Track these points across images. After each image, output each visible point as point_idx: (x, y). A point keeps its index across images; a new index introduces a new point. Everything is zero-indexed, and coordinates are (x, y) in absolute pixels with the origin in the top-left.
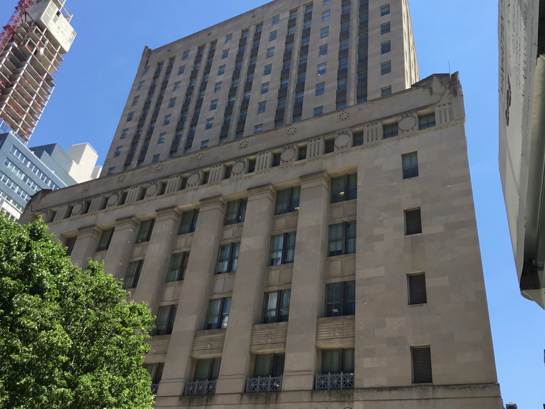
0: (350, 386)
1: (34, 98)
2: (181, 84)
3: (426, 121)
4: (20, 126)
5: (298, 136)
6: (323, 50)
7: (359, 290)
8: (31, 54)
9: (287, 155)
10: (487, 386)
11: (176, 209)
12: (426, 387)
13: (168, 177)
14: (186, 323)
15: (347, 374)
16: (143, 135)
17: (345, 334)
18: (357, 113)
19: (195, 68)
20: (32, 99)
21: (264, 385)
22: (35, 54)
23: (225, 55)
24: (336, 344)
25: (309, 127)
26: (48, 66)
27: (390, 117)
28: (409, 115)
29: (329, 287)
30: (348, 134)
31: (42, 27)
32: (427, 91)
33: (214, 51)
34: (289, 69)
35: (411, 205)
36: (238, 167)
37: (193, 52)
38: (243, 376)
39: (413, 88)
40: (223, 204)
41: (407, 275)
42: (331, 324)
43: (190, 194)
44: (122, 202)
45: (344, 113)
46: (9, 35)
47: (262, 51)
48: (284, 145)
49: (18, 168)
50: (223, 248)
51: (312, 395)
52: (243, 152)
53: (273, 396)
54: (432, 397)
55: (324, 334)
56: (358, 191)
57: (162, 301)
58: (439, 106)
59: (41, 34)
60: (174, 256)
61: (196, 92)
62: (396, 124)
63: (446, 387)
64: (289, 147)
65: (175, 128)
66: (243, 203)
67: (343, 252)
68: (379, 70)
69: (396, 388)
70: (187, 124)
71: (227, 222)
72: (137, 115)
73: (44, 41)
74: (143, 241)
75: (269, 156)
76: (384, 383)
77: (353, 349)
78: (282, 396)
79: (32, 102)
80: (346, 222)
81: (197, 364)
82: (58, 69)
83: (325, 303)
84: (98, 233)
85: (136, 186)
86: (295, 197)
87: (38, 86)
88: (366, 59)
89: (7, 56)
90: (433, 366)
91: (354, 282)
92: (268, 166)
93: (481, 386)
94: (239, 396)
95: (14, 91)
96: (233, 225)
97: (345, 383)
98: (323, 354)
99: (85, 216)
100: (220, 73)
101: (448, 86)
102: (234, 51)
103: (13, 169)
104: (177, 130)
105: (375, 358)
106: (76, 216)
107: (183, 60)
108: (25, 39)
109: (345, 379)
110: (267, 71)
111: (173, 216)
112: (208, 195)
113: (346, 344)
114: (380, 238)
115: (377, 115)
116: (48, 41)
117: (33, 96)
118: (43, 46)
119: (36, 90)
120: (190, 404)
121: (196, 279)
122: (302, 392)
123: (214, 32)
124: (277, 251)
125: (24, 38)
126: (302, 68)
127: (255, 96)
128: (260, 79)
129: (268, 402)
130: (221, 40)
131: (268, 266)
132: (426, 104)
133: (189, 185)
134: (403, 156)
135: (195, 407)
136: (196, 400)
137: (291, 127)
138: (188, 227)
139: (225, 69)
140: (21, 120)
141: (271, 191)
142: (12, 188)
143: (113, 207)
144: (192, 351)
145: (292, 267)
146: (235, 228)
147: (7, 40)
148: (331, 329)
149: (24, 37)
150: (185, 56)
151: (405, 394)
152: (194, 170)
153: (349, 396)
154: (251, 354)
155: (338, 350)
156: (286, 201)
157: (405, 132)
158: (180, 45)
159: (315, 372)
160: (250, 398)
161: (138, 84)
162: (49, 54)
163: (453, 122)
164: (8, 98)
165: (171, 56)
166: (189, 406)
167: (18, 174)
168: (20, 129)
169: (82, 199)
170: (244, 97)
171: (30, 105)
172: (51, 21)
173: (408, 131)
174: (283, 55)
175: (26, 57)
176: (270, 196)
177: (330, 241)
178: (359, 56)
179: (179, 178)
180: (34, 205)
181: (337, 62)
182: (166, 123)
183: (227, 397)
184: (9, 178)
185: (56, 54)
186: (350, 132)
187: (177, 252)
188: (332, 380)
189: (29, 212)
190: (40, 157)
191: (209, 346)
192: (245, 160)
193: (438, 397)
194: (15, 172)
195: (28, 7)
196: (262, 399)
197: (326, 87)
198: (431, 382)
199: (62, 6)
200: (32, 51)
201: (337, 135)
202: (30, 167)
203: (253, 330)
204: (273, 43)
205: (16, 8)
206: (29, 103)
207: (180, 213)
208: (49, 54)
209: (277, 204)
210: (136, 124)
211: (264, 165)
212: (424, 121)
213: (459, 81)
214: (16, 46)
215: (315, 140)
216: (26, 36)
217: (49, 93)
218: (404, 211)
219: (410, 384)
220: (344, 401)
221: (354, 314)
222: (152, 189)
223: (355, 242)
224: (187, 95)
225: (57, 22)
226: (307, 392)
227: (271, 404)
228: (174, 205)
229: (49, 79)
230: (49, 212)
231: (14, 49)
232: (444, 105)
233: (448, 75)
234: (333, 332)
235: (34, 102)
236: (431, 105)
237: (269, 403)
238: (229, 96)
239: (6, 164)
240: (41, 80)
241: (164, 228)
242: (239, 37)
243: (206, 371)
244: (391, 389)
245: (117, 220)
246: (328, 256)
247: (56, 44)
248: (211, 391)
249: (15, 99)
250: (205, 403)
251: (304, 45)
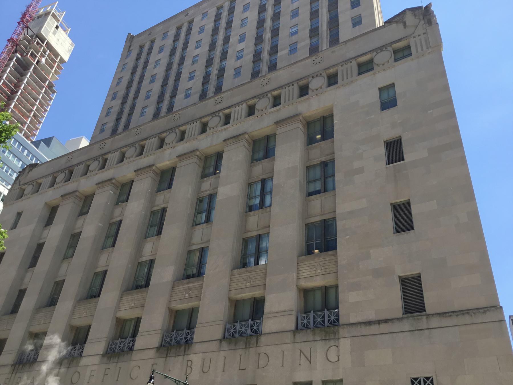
0: (335, 323)
1: (37, 103)
2: (161, 62)
3: (402, 53)
4: (25, 129)
5: (274, 85)
6: (295, 14)
7: (340, 225)
8: (33, 64)
9: (261, 104)
10: (488, 310)
11: (154, 168)
12: (420, 317)
13: (146, 139)
14: (164, 274)
15: (332, 311)
16: (126, 111)
17: (327, 270)
18: (330, 56)
19: (174, 46)
20: (35, 104)
21: (243, 329)
22: (37, 63)
23: (202, 30)
24: (319, 282)
25: (282, 76)
26: (50, 74)
27: (365, 54)
28: (384, 49)
29: (308, 227)
30: (322, 76)
31: (43, 39)
32: (401, 26)
33: (191, 29)
34: (263, 35)
35: (391, 135)
36: (213, 122)
37: (172, 32)
38: (221, 322)
39: (386, 25)
40: (200, 158)
41: (391, 204)
42: (311, 262)
43: (168, 152)
44: (103, 167)
45: (317, 57)
46: (12, 47)
47: (236, 22)
48: (258, 95)
49: (15, 156)
50: (200, 200)
51: (294, 335)
52: (219, 107)
53: (254, 340)
54: (426, 328)
55: (305, 272)
56: (335, 128)
57: (141, 257)
58: (414, 37)
59: (42, 46)
60: (153, 213)
61: (175, 67)
62: (371, 61)
63: (442, 315)
64: (263, 97)
65: (156, 101)
66: (219, 156)
67: (323, 191)
68: (350, 24)
69: (386, 321)
70: (167, 96)
71: (204, 176)
72: (121, 93)
73: (45, 52)
74: (122, 202)
75: (244, 108)
76: (372, 316)
77: (336, 287)
78: (263, 339)
79: (36, 107)
80: (324, 162)
81: (175, 315)
82: (59, 77)
83: (306, 243)
84: (81, 199)
85: (116, 150)
86: (271, 145)
87: (41, 93)
88: (337, 16)
89: (11, 66)
90: (425, 295)
91: (334, 219)
92: (243, 117)
93: (481, 311)
94: (217, 343)
95: (19, 98)
96: (211, 177)
97: (329, 320)
98: (305, 293)
99: (68, 184)
100: (197, 47)
101: (421, 17)
102: (210, 26)
103: (11, 157)
104: (158, 103)
105: (361, 291)
106: (60, 185)
107: (162, 40)
108: (28, 50)
109: (329, 317)
110: (242, 39)
111: (151, 174)
112: (186, 151)
113: (329, 281)
114: (361, 171)
115: (352, 54)
116: (48, 52)
117: (36, 101)
118: (44, 57)
119: (39, 96)
120: (167, 355)
121: (173, 232)
122: (283, 333)
123: (191, 12)
124: (255, 197)
125: (26, 49)
126: (275, 32)
127: (231, 64)
128: (235, 46)
129: (248, 347)
130: (197, 19)
131: (246, 212)
132: (400, 38)
133: (167, 144)
134: (380, 90)
135: (173, 358)
136: (173, 351)
137: (265, 78)
138: (166, 184)
139: (202, 43)
140: (26, 123)
141: (246, 140)
142: (10, 174)
143: (94, 173)
144: (170, 301)
145: (270, 211)
146: (213, 180)
147: (11, 51)
148: (312, 267)
149: (26, 49)
150: (165, 36)
151: (396, 327)
152: (171, 130)
153: (334, 333)
154: (230, 300)
155: (320, 288)
156: (263, 148)
157: (381, 66)
158: (161, 28)
159: (297, 313)
160: (230, 344)
161: (122, 66)
162: (51, 63)
163: (430, 50)
164: (14, 104)
165: (152, 38)
166: (166, 357)
167: (15, 161)
168: (25, 131)
169: (65, 169)
170: (221, 66)
171: (34, 109)
172: (51, 34)
173: (383, 64)
174: (256, 23)
175: (29, 66)
176: (246, 145)
177: (308, 182)
178: (330, 14)
179: (157, 138)
180: (23, 180)
181: (308, 23)
182: (148, 97)
183: (205, 345)
184: (6, 165)
185: (57, 64)
186: (324, 74)
187: (156, 208)
188: (315, 318)
189: (17, 186)
190: (37, 148)
191: (187, 295)
192: (221, 114)
193: (434, 327)
194: (13, 159)
195: (29, 21)
196: (242, 344)
197: (299, 46)
198: (425, 311)
199: (61, 20)
200: (34, 61)
201: (311, 78)
202: (27, 155)
203: (232, 275)
204: (247, 14)
205: (19, 23)
206: (33, 108)
207: (158, 171)
208: (51, 63)
209: (254, 152)
210: (120, 101)
211: (239, 116)
212: (400, 55)
213: (433, 12)
214: (20, 56)
215: (289, 87)
216: (28, 48)
217: (51, 99)
218: (384, 142)
219: (400, 315)
220: (329, 339)
221: (336, 249)
222: (130, 152)
223: (334, 181)
224: (166, 70)
225: (56, 35)
226: (289, 333)
227: (251, 349)
228: (152, 163)
229: (50, 86)
230: (35, 184)
231: (18, 60)
232: (419, 35)
233: (420, 8)
234: (315, 269)
235: (37, 106)
236: (406, 37)
237: (250, 348)
238: (206, 67)
239: (4, 152)
240: (44, 87)
241: (143, 187)
242: (215, 13)
243: (184, 322)
244: (379, 322)
245: (98, 184)
246: (306, 197)
247: (57, 55)
248: (190, 340)
249: (19, 104)
250: (182, 353)
251: (277, 11)
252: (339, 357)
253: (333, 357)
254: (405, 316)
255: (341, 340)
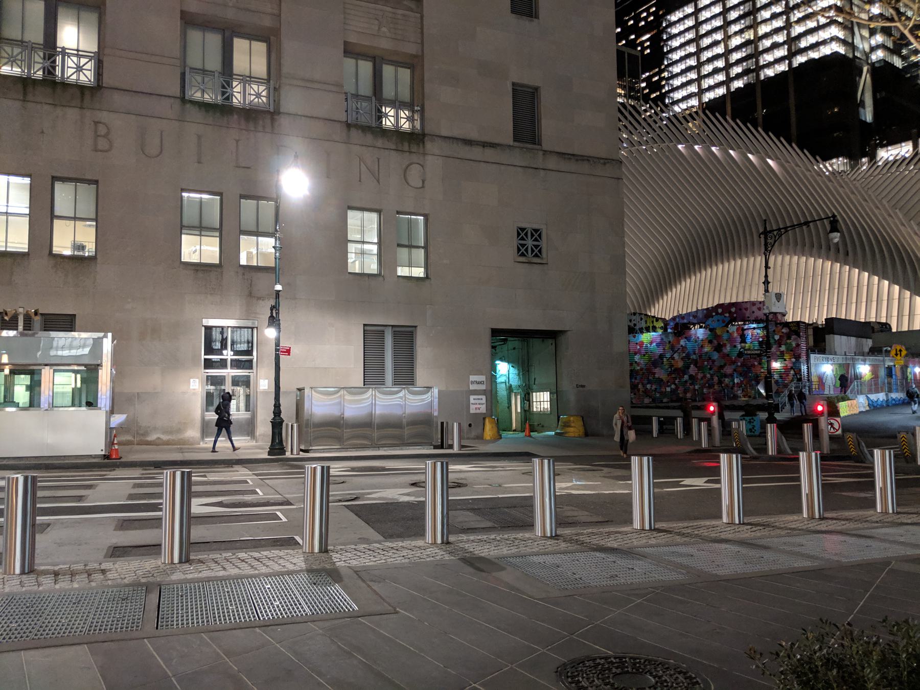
51: (349, 130)
63: (561, 155)
69: (493, 145)
76: (474, 135)
93: (602, 161)
135: (46, 107)
244: (485, 145)
252: (423, 182)
253: (416, 181)
254: (516, 144)
255: (429, 158)
